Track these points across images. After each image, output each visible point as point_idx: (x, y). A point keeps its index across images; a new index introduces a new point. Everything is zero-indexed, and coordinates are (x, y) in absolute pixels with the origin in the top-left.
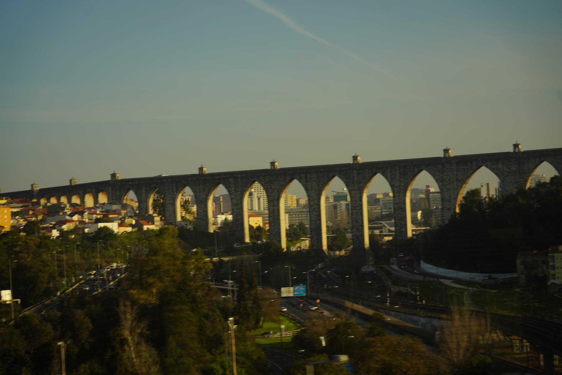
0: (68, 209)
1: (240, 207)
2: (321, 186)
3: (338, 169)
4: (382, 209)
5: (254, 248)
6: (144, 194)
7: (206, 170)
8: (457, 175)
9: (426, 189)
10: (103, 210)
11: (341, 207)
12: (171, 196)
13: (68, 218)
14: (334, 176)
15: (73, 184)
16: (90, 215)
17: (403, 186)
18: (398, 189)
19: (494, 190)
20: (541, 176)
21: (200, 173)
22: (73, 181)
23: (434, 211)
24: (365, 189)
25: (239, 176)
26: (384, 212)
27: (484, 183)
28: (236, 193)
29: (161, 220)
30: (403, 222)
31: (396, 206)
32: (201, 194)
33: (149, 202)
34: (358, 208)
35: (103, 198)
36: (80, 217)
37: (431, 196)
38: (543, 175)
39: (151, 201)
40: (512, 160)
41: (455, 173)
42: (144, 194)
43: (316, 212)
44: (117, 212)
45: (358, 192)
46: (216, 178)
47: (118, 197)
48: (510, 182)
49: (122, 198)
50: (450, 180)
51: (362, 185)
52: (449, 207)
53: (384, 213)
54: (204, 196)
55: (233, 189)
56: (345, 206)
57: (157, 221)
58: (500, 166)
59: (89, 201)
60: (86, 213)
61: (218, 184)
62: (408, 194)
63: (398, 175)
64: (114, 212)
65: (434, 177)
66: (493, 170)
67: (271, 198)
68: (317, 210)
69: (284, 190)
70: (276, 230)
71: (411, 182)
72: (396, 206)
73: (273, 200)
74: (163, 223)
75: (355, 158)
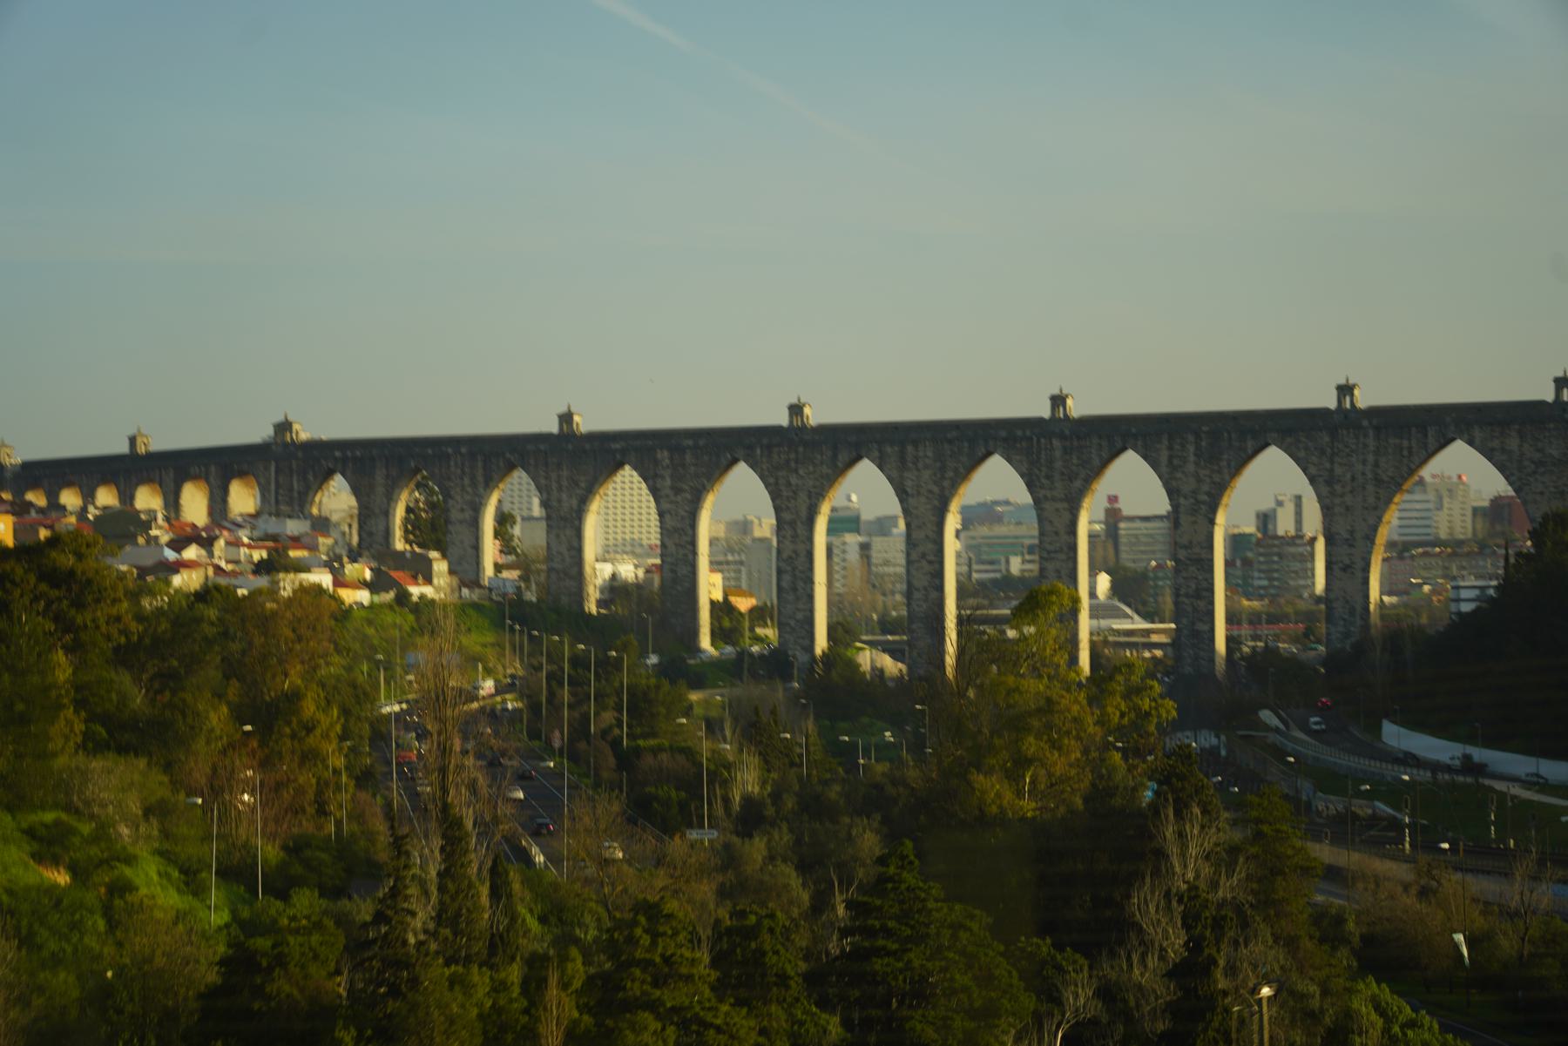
0: (160, 528)
1: (688, 539)
2: (946, 483)
3: (1003, 434)
4: (970, 566)
5: (736, 668)
6: (380, 490)
7: (814, 416)
8: (1376, 465)
9: (1108, 505)
10: (256, 534)
11: (844, 552)
12: (468, 498)
13: (170, 555)
14: (988, 454)
15: (141, 450)
16: (232, 549)
17: (1208, 494)
18: (1192, 501)
19: (1253, 520)
20: (1455, 479)
21: (791, 422)
22: (139, 441)
23: (1151, 575)
24: (1084, 497)
25: (690, 442)
26: (978, 571)
27: (1285, 495)
28: (676, 495)
29: (451, 572)
30: (1202, 604)
31: (1182, 554)
32: (564, 496)
33: (394, 516)
34: (1062, 556)
35: (243, 499)
36: (203, 552)
37: (1125, 529)
38: (1460, 477)
39: (400, 512)
40: (1552, 426)
41: (1371, 458)
42: (380, 490)
43: (930, 562)
44: (305, 540)
45: (1066, 505)
46: (617, 446)
47: (296, 495)
48: (1542, 493)
49: (310, 498)
50: (1353, 479)
51: (1078, 484)
52: (1347, 561)
53: (975, 576)
54: (575, 502)
55: (668, 482)
56: (857, 548)
57: (440, 574)
58: (1513, 443)
59: (195, 505)
60: (221, 542)
61: (619, 466)
62: (952, 522)
63: (1192, 458)
64: (296, 541)
65: (1305, 470)
66: (1488, 454)
67: (787, 516)
68: (931, 558)
69: (828, 492)
70: (800, 616)
71: (1230, 482)
72: (1182, 554)
73: (792, 524)
74: (455, 581)
75: (1345, 390)
